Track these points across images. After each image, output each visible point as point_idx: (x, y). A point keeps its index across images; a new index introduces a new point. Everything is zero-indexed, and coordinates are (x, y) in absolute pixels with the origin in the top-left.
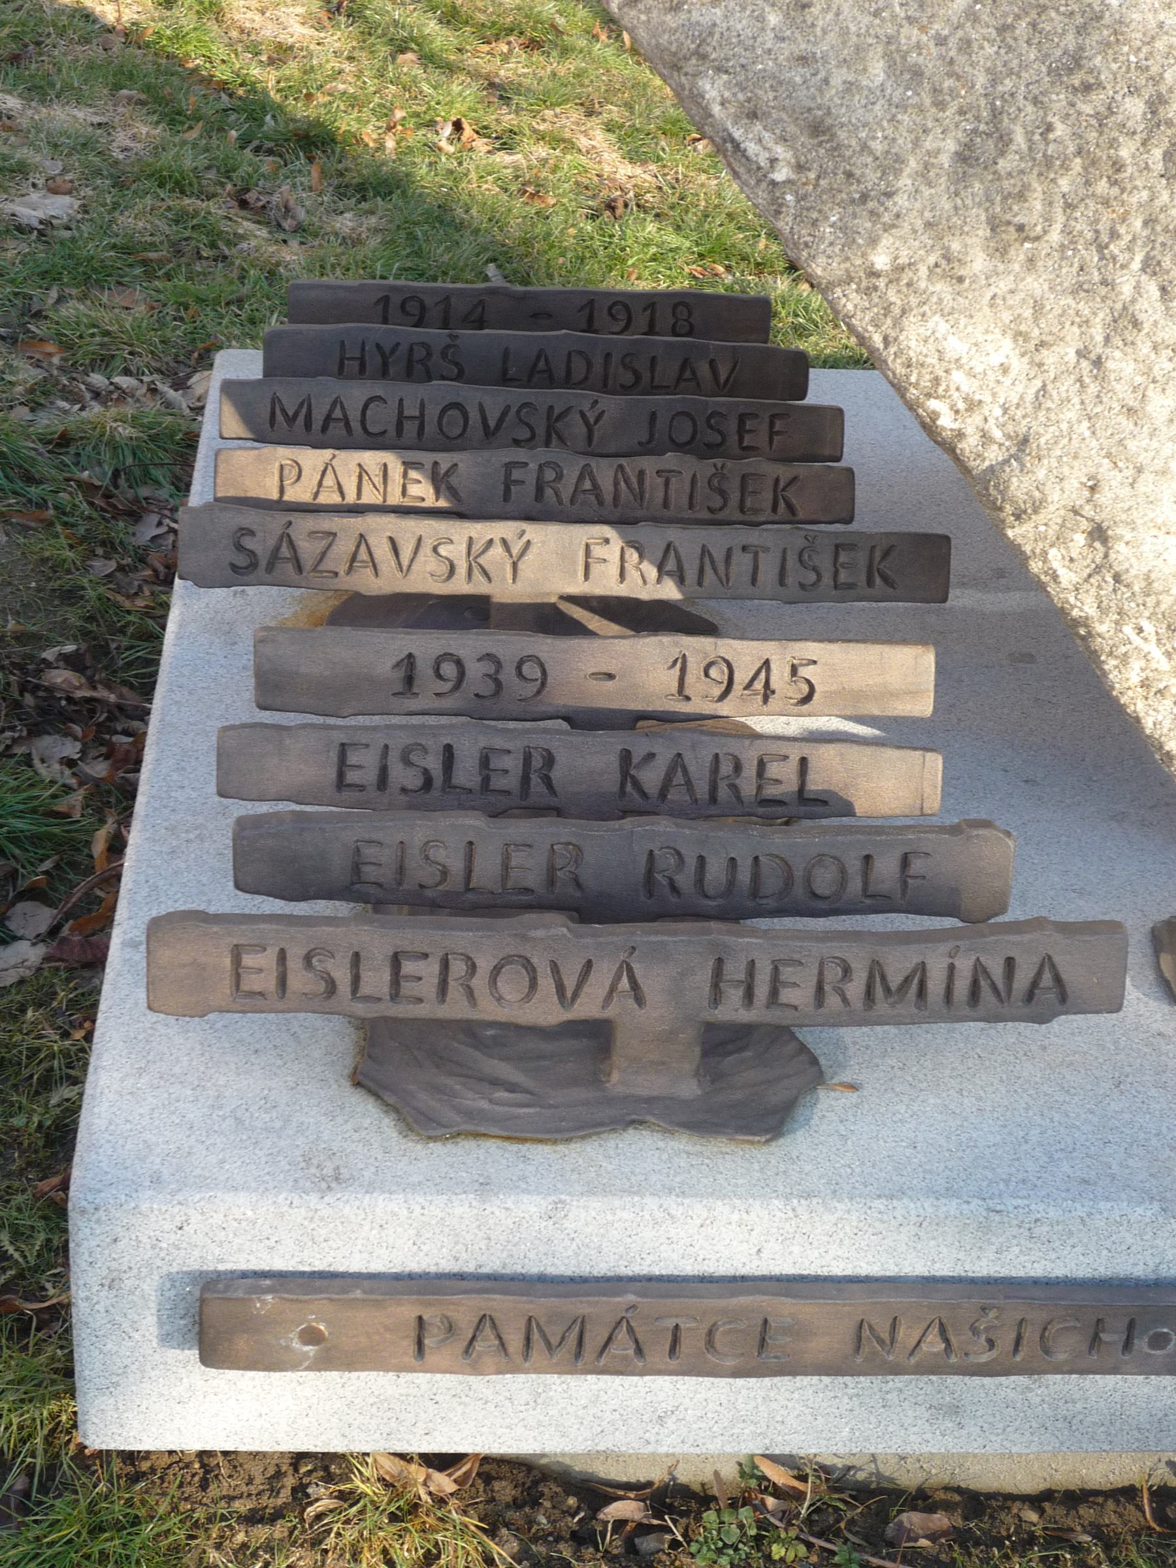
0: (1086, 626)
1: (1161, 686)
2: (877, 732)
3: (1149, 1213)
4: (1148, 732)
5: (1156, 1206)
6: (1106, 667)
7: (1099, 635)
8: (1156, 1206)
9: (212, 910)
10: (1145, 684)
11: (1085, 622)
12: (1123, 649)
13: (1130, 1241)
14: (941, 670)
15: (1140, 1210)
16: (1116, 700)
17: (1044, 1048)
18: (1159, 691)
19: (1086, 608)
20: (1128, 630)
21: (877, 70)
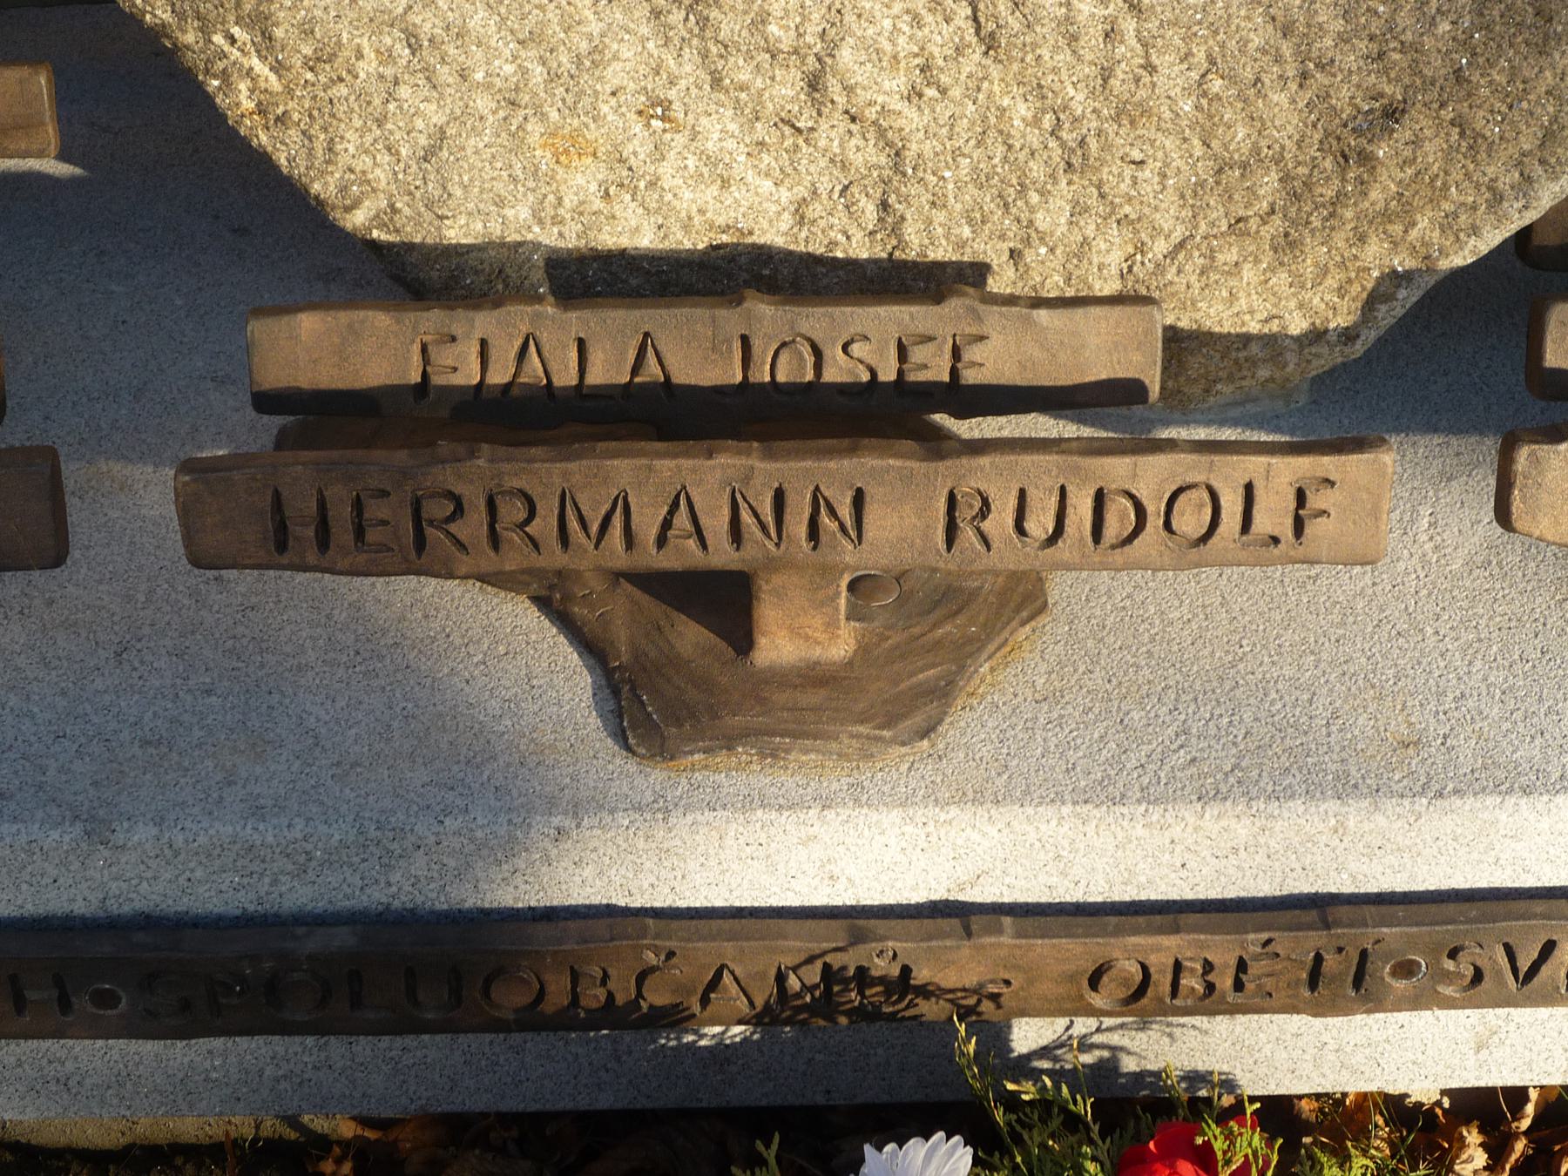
0: (169, 37)
1: (280, 111)
2: (78, 171)
3: (67, 838)
4: (285, 171)
5: (78, 828)
6: (210, 89)
7: (187, 47)
8: (78, 828)
9: (634, 230)
10: (261, 110)
11: (160, 31)
12: (220, 65)
13: (53, 872)
14: (63, 97)
15: (55, 835)
16: (233, 132)
17: (50, 602)
18: (278, 119)
19: (159, 12)
20: (218, 39)
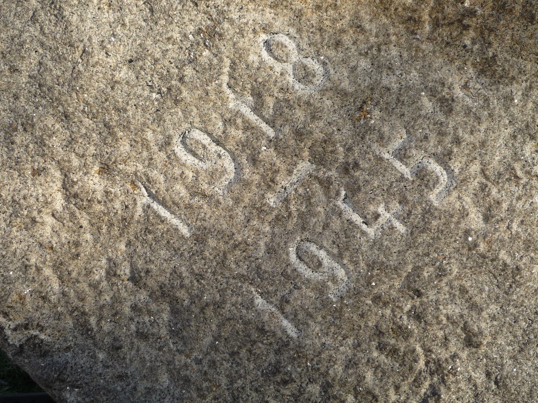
21: (164, 379)
